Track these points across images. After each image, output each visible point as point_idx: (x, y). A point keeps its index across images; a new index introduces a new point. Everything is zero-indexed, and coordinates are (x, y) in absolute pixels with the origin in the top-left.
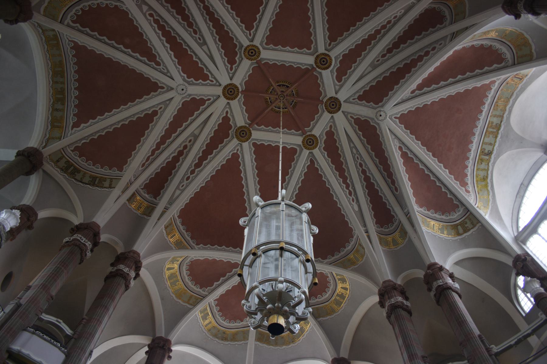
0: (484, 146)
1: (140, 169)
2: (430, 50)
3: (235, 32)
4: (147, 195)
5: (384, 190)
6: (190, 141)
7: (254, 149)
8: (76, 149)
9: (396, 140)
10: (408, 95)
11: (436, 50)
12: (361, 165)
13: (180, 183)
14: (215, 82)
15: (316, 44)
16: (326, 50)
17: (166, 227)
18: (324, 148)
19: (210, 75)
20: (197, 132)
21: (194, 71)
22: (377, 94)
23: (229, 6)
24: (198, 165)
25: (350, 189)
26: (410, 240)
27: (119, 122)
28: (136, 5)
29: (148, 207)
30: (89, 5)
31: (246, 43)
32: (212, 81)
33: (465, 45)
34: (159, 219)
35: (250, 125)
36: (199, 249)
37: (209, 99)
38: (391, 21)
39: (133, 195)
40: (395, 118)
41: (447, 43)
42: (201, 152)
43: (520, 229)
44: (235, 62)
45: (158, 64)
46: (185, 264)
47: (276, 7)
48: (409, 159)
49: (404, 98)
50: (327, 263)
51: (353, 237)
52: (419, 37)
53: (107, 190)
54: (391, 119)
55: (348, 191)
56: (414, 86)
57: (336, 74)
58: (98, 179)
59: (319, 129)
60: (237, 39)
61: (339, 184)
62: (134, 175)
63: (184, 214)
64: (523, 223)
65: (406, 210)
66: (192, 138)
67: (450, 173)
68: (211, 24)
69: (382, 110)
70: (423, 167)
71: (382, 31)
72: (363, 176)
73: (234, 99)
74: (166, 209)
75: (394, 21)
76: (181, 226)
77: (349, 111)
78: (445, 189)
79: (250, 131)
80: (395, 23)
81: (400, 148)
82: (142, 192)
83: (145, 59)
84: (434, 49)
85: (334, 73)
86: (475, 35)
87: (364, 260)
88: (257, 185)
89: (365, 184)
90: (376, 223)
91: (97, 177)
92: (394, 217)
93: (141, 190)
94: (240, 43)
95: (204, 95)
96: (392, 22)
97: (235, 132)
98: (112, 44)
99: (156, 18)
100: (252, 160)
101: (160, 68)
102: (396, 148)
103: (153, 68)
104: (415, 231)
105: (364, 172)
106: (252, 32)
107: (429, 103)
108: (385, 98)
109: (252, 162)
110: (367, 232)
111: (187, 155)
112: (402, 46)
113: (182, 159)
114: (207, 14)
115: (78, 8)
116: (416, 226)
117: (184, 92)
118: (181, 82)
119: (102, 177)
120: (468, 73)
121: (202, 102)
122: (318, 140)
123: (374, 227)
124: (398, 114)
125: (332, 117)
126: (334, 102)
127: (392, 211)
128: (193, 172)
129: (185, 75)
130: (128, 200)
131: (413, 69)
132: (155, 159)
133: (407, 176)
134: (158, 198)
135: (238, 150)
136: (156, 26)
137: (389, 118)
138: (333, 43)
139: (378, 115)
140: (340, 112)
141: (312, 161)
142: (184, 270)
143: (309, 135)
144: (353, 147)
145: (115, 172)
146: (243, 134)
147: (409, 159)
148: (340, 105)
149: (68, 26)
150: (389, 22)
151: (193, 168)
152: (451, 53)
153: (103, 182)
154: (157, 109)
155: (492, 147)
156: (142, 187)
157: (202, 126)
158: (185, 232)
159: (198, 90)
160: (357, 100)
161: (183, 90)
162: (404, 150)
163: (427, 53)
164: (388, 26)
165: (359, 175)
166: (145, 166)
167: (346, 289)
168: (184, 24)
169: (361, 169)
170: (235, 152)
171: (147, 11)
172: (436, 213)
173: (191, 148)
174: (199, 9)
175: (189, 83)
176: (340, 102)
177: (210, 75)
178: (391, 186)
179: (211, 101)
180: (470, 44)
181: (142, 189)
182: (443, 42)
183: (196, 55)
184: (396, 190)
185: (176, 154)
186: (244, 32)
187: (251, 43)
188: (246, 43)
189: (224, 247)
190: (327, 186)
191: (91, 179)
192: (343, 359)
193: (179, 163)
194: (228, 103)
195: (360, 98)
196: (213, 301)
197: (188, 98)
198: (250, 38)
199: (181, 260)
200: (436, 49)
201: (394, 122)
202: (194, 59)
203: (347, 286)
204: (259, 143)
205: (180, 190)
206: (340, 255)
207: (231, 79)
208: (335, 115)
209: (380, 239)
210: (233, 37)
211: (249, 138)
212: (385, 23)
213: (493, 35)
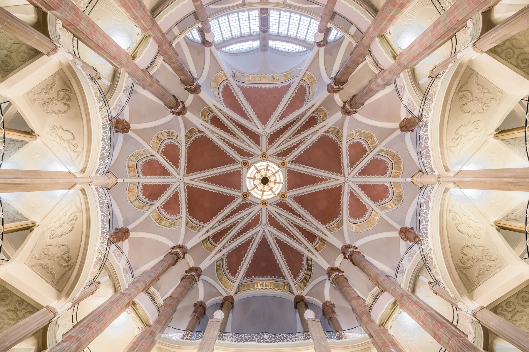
8: (294, 278)
17: (331, 231)
20: (285, 218)
21: (255, 222)
24: (300, 216)
31: (241, 199)
39: (315, 249)
43: (304, 49)
45: (253, 238)
48: (283, 116)
62: (306, 248)
64: (301, 49)
82: (314, 244)
105: (293, 136)
115: (228, 275)
121: (270, 216)
128: (303, 219)
145: (304, 258)
147: (283, 116)
149: (236, 279)
150: (221, 139)
155: (393, 85)
159: (264, 219)
163: (231, 119)
167: (356, 133)
175: (261, 223)
184: (298, 118)
188: (241, 199)
195: (259, 144)
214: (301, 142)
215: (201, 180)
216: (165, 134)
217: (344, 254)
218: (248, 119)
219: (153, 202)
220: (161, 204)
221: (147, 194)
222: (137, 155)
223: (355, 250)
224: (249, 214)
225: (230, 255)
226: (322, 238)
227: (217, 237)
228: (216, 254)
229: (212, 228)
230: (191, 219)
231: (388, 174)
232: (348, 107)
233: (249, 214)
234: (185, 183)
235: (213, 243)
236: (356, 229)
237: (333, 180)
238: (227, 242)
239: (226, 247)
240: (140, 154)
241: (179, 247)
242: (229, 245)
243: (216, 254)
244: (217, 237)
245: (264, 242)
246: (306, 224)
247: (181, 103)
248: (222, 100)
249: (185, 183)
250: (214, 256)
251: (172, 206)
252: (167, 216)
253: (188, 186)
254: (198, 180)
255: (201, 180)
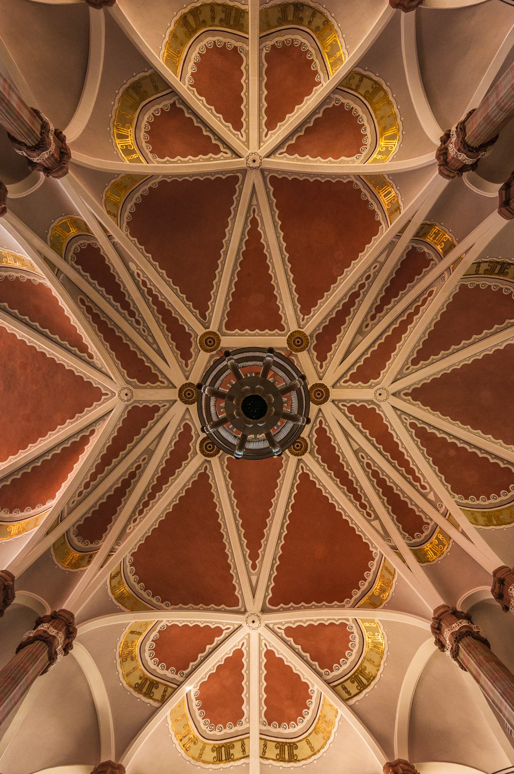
0: (161, 688)
1: (435, 289)
2: (84, 491)
3: (321, 471)
4: (426, 250)
5: (98, 296)
6: (367, 326)
7: (282, 322)
9: (99, 366)
10: (98, 427)
11: (78, 492)
12: (138, 322)
13: (379, 271)
14: (340, 405)
15: (222, 466)
16: (209, 462)
17: (398, 209)
18: (191, 336)
19: (347, 412)
21: (366, 417)
22: (138, 419)
23: (330, 501)
25: (146, 290)
26: (44, 238)
27: (463, 348)
28: (442, 502)
29: (425, 235)
30: (499, 496)
32: (343, 405)
33: (43, 507)
34: (410, 221)
35: (291, 354)
36: (348, 176)
37: (345, 382)
38: (139, 515)
40: (107, 394)
41: (66, 507)
42: (352, 313)
44: (316, 432)
45: (413, 425)
46: (368, 147)
47: (276, 505)
49: (101, 422)
50: (157, 176)
51: (128, 223)
52: (102, 501)
53: (483, 259)
54: (112, 392)
55: (149, 286)
56: (94, 440)
57: (193, 433)
58: (496, 271)
59: (202, 360)
60: (318, 461)
61: (161, 294)
62: (443, 279)
63: (372, 228)
65: (61, 277)
66: (365, 330)
67: (14, 335)
68: (350, 477)
69: (126, 403)
70: (54, 336)
71: (146, 499)
72: (132, 308)
73: (313, 385)
74: (398, 236)
75: (135, 515)
76: (376, 210)
77: (167, 391)
78: (15, 313)
79: (289, 347)
80: (134, 512)
81: (91, 356)
82: (433, 256)
83: (429, 431)
84: (80, 494)
85: (194, 433)
86: (35, 526)
87: (104, 193)
88: (272, 275)
89: (127, 299)
90: (98, 250)
91: (497, 274)
92: (76, 263)
93: (434, 258)
94: (314, 457)
95: (353, 387)
96: (137, 513)
97: (308, 343)
98: (471, 448)
99: (418, 484)
100: (283, 307)
101: (410, 419)
102: (97, 356)
103: (418, 420)
104: (39, 253)
105: (132, 314)
106: (301, 472)
107: (68, 421)
108: (126, 416)
109: (283, 305)
110: (110, 237)
111: (371, 308)
112: (119, 485)
113: (377, 302)
114: (356, 489)
116: (41, 261)
117: (379, 392)
118: (382, 404)
119: (490, 274)
120: (29, 471)
121: (354, 378)
122: (201, 346)
123: (101, 244)
124: (105, 399)
125: (187, 379)
126: (188, 398)
127: (81, 271)
129: (378, 411)
130: (455, 246)
131: (99, 461)
132: (415, 301)
133: (72, 323)
134: (411, 248)
135: (303, 320)
136: (417, 474)
137: (115, 396)
138: (203, 471)
139: (130, 394)
140: (179, 387)
141: (204, 317)
142: (369, 135)
143: (212, 351)
144: (153, 344)
145: (470, 284)
146: (298, 341)
148: (180, 396)
150: (141, 512)
151: (361, 291)
152: (59, 494)
153: (489, 268)
154: (412, 367)
156: (432, 262)
157: (353, 346)
158: (370, 199)
160: (160, 406)
161: (380, 394)
162: (85, 355)
164: (141, 507)
165: (137, 309)
166: (429, 292)
167: (121, 137)
168: (383, 475)
169: (137, 317)
170: (306, 317)
171: (429, 493)
172: (17, 277)
173: (366, 317)
174: (366, 496)
175: (372, 402)
176: (181, 400)
177: (347, 412)
178: (90, 304)
179: (343, 380)
180: (37, 510)
181: (432, 260)
182: (71, 506)
183: (366, 437)
185: (386, 307)
186: (310, 470)
187: (300, 457)
189: (312, 180)
190: (178, 288)
191: (506, 270)
192: (97, 6)
193: (381, 296)
194: (321, 380)
196: (322, 81)
197: (372, 383)
198: (301, 464)
199: (375, 156)
200: (77, 495)
201: (108, 389)
202: (367, 431)
203: (119, 144)
204: (276, 330)
205: (379, 262)
206: (140, 192)
207: (320, 410)
208: (185, 381)
209: (88, 230)
210: (322, 464)
211: (289, 336)
212: (145, 510)
213: (14, 528)
214: (150, 291)
215: (254, 567)
216: (129, 665)
217: (463, 168)
218: (85, 440)
219: (314, 696)
220: (320, 675)
221: (292, 711)
222: (185, 740)
223: (454, 139)
224: (346, 434)
225: (459, 487)
226: (417, 234)
227: (410, 522)
228: (456, 526)
229: (386, 536)
230: (359, 593)
231: (238, 44)
232: (45, 155)
233: (346, 434)
234: (264, 610)
235: (426, 533)
236: (393, 137)
237: (254, 202)
238: (425, 496)
239: (436, 495)
240: (184, 732)
241: (437, 629)
242: (431, 489)
243: (456, 526)
244: (410, 522)
245: (422, 394)
246: (375, 276)
247: (40, 628)
248: (32, 512)
249: (264, 610)
250: (463, 533)
251: (323, 647)
252: (351, 659)
253: (271, 602)
254: (254, 576)
255: (254, 567)
